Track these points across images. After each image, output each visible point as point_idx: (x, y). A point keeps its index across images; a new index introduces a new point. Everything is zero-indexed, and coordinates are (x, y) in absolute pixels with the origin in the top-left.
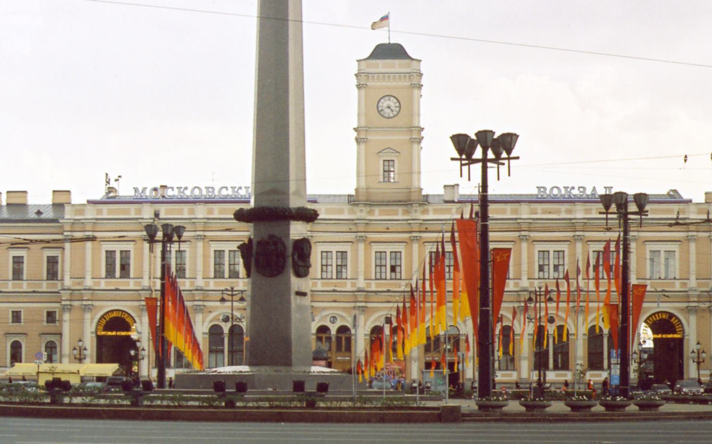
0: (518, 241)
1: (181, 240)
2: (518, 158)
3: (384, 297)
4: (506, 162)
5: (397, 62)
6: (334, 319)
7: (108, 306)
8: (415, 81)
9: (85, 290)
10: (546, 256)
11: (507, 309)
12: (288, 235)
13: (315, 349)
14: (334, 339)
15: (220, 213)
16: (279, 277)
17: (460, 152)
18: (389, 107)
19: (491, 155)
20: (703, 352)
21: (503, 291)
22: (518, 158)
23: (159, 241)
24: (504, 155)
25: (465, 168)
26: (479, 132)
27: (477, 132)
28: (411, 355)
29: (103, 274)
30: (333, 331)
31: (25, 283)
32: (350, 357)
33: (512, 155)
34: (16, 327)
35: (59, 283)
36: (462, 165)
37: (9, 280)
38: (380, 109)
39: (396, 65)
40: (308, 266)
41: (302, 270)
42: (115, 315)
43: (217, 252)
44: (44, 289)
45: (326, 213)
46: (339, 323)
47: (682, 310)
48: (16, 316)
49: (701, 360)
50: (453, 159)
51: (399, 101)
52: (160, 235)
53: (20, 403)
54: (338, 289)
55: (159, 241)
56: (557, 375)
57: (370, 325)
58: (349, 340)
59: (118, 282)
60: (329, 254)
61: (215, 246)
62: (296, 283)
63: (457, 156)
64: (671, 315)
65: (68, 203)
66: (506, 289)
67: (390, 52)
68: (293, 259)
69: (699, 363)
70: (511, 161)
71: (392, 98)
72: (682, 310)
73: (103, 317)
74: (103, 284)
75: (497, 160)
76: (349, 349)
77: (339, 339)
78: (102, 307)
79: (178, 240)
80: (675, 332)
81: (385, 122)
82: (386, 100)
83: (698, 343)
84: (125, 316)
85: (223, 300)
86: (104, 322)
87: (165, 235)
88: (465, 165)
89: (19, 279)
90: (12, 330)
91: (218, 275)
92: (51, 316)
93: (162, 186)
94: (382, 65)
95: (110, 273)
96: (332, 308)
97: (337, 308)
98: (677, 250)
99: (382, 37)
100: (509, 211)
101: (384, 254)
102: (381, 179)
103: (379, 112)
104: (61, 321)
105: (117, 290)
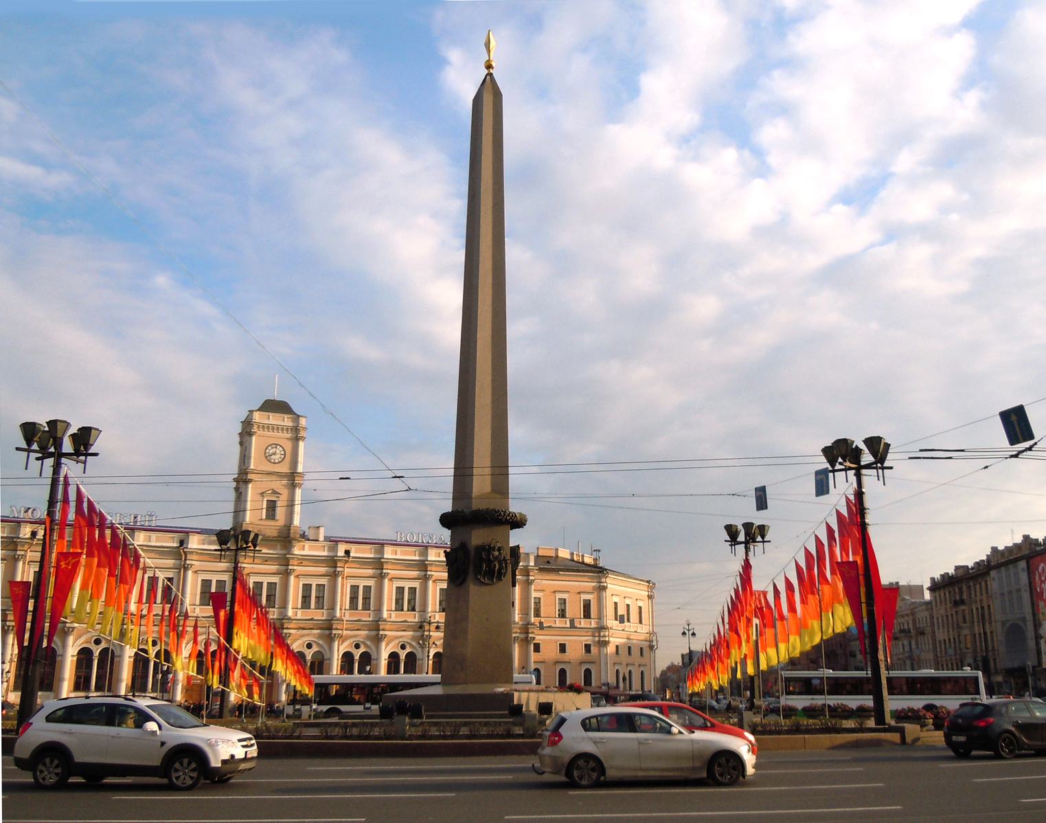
1: (765, 540)
5: (286, 416)
6: (403, 647)
10: (309, 588)
12: (471, 542)
13: (54, 639)
22: (769, 541)
23: (741, 543)
24: (759, 539)
27: (823, 447)
28: (844, 608)
33: (765, 540)
38: (267, 455)
39: (287, 421)
43: (413, 590)
45: (355, 552)
50: (726, 541)
51: (284, 450)
52: (741, 538)
53: (359, 737)
55: (741, 543)
60: (322, 587)
61: (303, 581)
63: (729, 539)
70: (885, 470)
71: (278, 447)
82: (273, 448)
87: (747, 534)
91: (322, 587)
94: (274, 419)
101: (223, 583)
103: (266, 457)
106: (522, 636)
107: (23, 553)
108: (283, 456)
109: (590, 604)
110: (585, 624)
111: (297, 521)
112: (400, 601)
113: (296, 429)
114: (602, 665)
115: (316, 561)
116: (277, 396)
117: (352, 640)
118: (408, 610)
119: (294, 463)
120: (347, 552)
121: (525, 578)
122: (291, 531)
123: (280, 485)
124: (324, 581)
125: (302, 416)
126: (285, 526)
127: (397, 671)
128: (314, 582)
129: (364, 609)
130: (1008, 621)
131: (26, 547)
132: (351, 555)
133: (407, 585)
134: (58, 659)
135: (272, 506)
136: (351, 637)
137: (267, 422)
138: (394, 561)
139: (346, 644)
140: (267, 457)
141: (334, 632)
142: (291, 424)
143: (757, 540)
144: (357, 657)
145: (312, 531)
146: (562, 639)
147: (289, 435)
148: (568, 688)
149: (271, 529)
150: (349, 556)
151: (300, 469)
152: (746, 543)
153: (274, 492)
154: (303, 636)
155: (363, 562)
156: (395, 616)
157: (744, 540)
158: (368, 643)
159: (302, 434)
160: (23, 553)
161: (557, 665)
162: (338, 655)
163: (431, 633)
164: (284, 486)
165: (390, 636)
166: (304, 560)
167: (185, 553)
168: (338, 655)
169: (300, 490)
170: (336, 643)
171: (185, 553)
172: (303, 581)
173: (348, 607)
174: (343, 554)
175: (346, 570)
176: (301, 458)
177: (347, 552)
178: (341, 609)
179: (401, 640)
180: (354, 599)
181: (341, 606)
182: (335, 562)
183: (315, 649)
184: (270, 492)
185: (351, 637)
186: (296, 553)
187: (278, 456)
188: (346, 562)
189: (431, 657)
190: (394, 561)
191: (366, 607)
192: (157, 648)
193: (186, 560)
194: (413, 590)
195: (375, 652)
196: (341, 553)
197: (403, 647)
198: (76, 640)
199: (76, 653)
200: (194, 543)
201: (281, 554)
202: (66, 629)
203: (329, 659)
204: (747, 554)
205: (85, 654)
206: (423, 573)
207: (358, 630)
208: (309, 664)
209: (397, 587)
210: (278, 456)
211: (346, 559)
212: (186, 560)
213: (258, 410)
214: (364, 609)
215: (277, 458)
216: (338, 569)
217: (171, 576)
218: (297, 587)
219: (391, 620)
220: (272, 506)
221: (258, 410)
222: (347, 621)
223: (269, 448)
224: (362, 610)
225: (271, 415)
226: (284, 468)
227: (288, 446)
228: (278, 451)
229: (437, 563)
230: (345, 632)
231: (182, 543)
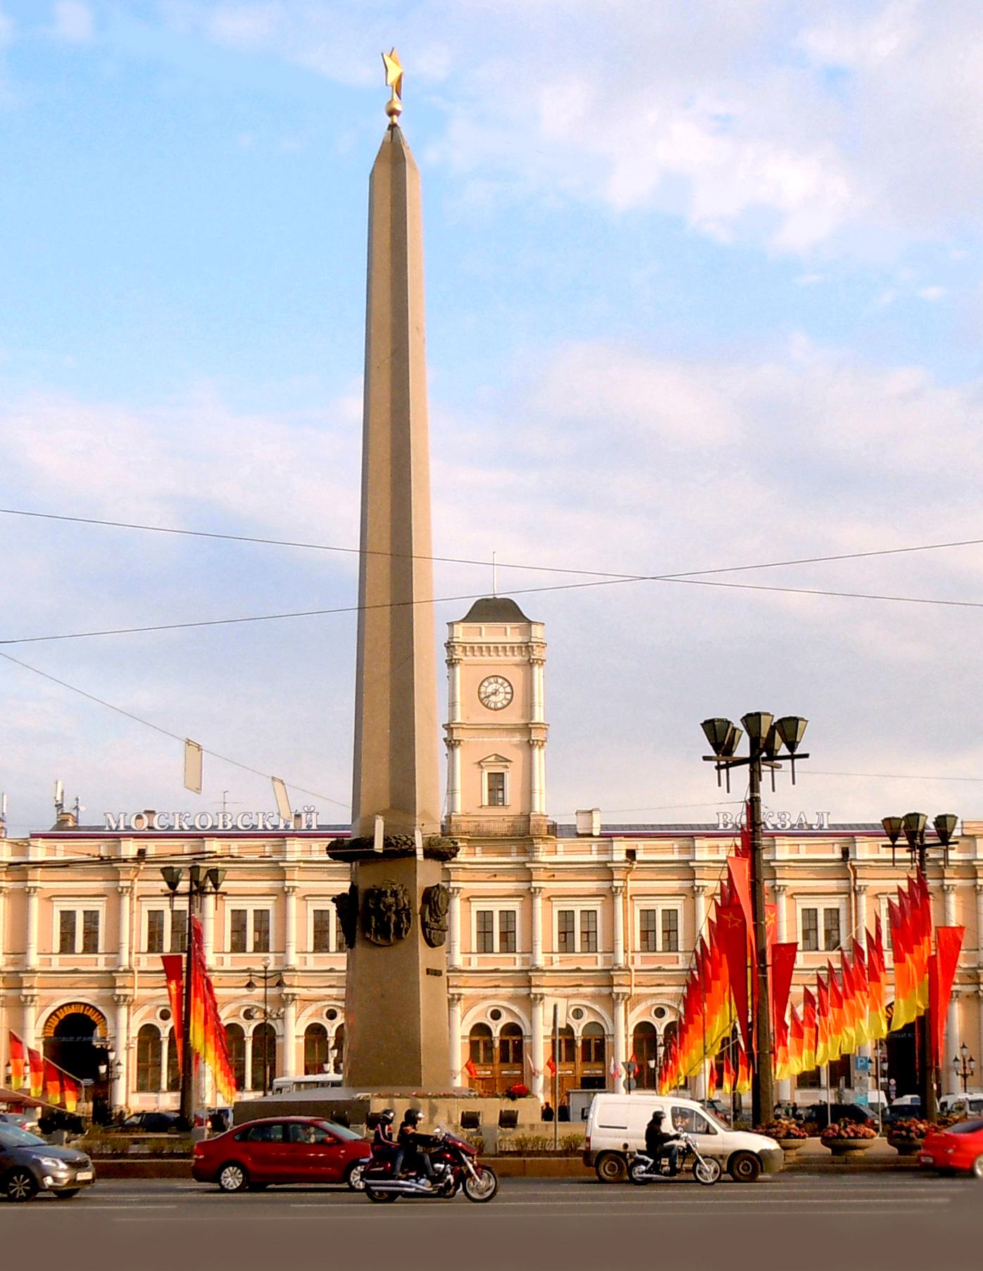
0: (528, 897)
1: (796, 753)
2: (806, 756)
4: (786, 764)
5: (509, 626)
6: (496, 1015)
7: (61, 997)
8: (529, 657)
9: (27, 972)
16: (402, 945)
17: (716, 746)
18: (494, 694)
20: (971, 1060)
21: (793, 969)
22: (806, 756)
24: (783, 750)
25: (723, 772)
26: (749, 715)
29: (57, 948)
30: (496, 1033)
32: (604, 1070)
33: (796, 753)
36: (719, 768)
39: (509, 633)
40: (444, 930)
41: (436, 934)
42: (73, 1010)
43: (813, 913)
46: (505, 1019)
49: (968, 1072)
50: (705, 758)
52: (743, 749)
56: (142, 1100)
57: (636, 1017)
58: (519, 1049)
59: (79, 959)
62: (426, 956)
63: (713, 754)
66: (796, 966)
68: (423, 919)
69: (965, 1076)
70: (796, 761)
73: (54, 1013)
74: (57, 962)
75: (772, 757)
76: (519, 1057)
77: (504, 1044)
78: (52, 999)
79: (788, 753)
83: (964, 1047)
84: (89, 1013)
85: (250, 985)
86: (55, 1022)
88: (723, 767)
93: (146, 812)
94: (490, 632)
95: (67, 945)
102: (486, 802)
103: (481, 700)
106: (970, 989)
107: (128, 884)
108: (509, 696)
110: (315, 963)
111: (540, 806)
112: (812, 934)
113: (527, 647)
115: (580, 870)
116: (500, 591)
117: (650, 1002)
118: (827, 949)
119: (529, 706)
120: (631, 854)
121: (969, 883)
122: (532, 823)
123: (508, 745)
124: (835, 903)
125: (536, 623)
126: (521, 815)
128: (577, 907)
129: (257, 949)
131: (132, 874)
132: (638, 857)
133: (821, 904)
134: (278, 1041)
135: (497, 781)
138: (712, 865)
139: (640, 1009)
140: (484, 701)
141: (616, 990)
142: (519, 639)
143: (779, 754)
144: (660, 1031)
145: (583, 818)
147: (518, 658)
148: (922, 1089)
149: (499, 820)
150: (634, 859)
151: (539, 717)
152: (753, 761)
153: (501, 759)
154: (485, 998)
155: (661, 868)
156: (558, 962)
157: (747, 755)
158: (516, 1009)
159: (537, 654)
160: (128, 884)
162: (627, 1029)
164: (516, 745)
165: (467, 998)
166: (554, 872)
167: (853, 867)
168: (627, 1029)
169: (543, 751)
170: (622, 1008)
171: (853, 867)
172: (231, 904)
173: (638, 948)
174: (623, 857)
175: (630, 884)
176: (539, 698)
177: (631, 854)
178: (625, 951)
179: (245, 1001)
180: (647, 935)
181: (626, 945)
182: (610, 870)
183: (587, 1018)
184: (492, 759)
186: (543, 859)
187: (502, 696)
188: (629, 870)
189: (631, 1031)
190: (712, 865)
191: (91, 947)
192: (254, 1024)
193: (855, 878)
194: (91, 917)
195: (527, 1024)
196: (620, 856)
199: (302, 1033)
200: (865, 851)
201: (598, 862)
202: (23, 999)
203: (531, 1037)
204: (754, 787)
206: (688, 884)
207: (659, 985)
208: (579, 1044)
209: (233, 911)
210: (502, 696)
211: (627, 865)
212: (855, 878)
213: (464, 620)
214: (257, 949)
215: (499, 700)
216: (616, 883)
217: (836, 906)
219: (307, 968)
220: (497, 781)
221: (464, 620)
222: (140, 972)
223: (486, 684)
224: (664, 951)
225: (483, 626)
226: (513, 717)
227: (517, 676)
228: (501, 690)
229: (792, 864)
230: (636, 991)
231: (845, 852)
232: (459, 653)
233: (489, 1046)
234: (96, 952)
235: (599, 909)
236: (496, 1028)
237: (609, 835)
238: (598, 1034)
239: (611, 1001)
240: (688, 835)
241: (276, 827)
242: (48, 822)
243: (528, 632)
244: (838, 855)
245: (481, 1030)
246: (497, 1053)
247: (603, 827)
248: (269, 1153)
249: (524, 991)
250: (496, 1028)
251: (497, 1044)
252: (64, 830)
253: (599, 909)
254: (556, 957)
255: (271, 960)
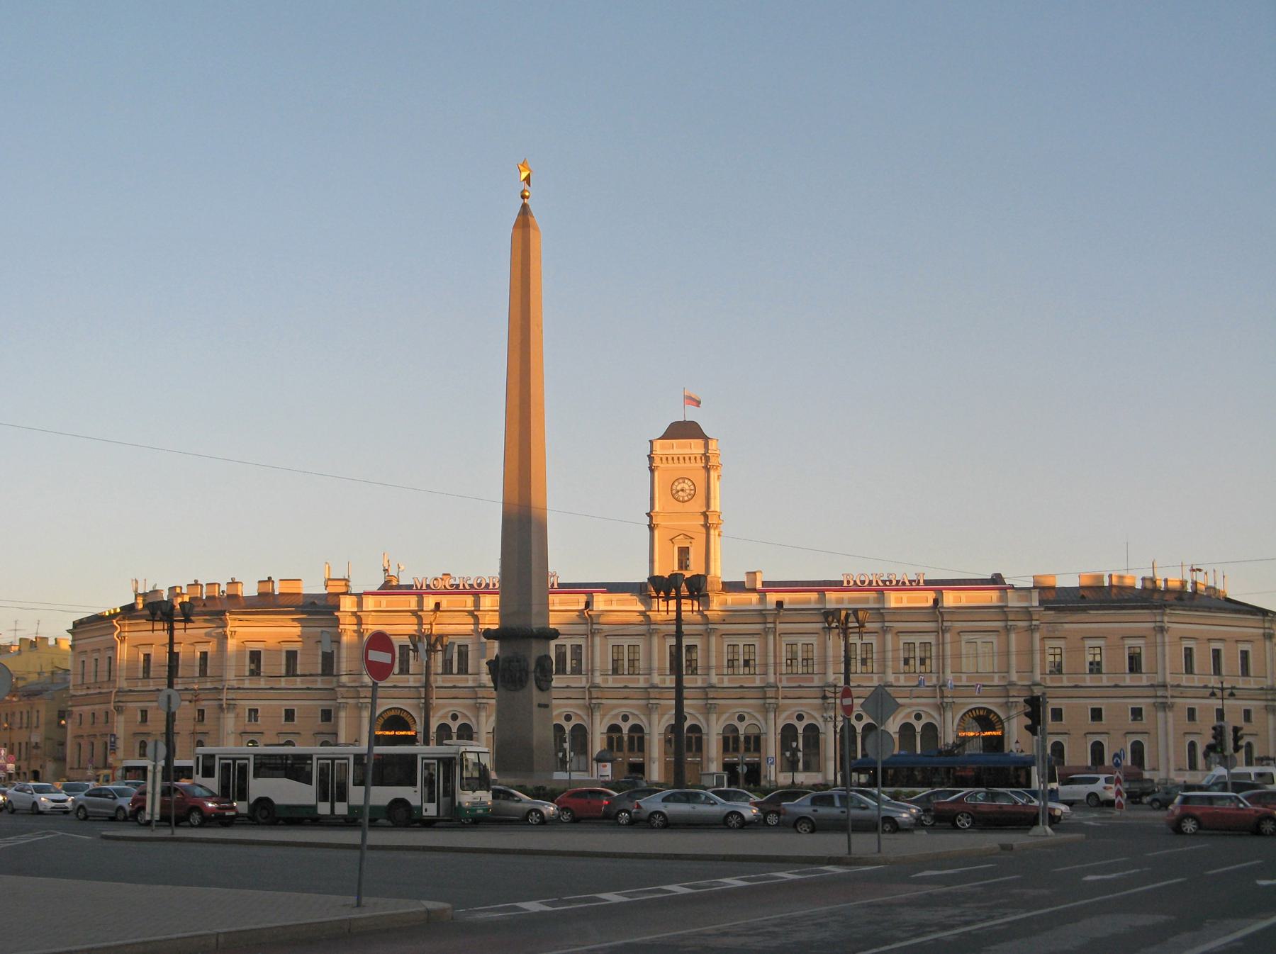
3: (567, 693)
11: (692, 706)
14: (626, 738)
15: (561, 604)
19: (662, 594)
29: (141, 675)
30: (625, 730)
31: (1104, 677)
34: (1096, 726)
35: (335, 679)
37: (317, 675)
39: (696, 446)
42: (393, 713)
44: (319, 686)
47: (1001, 705)
48: (290, 715)
54: (630, 685)
57: (607, 722)
58: (641, 740)
61: (728, 641)
64: (990, 711)
65: (345, 593)
67: (683, 430)
72: (1001, 705)
76: (641, 749)
77: (631, 739)
80: (409, 730)
81: (679, 507)
84: (404, 715)
89: (331, 674)
90: (249, 729)
92: (327, 715)
96: (566, 706)
97: (571, 706)
98: (995, 641)
99: (691, 414)
100: (905, 599)
104: (337, 717)
105: (454, 687)
109: (332, 658)
113: (706, 457)
114: (1161, 733)
115: (762, 614)
127: (736, 749)
129: (574, 671)
130: (339, 649)
135: (684, 552)
136: (910, 705)
137: (671, 452)
144: (918, 729)
146: (1096, 703)
161: (1129, 736)
163: (781, 701)
177: (438, 605)
185: (910, 705)
195: (763, 722)
197: (918, 717)
198: (718, 720)
205: (788, 733)
213: (662, 438)
218: (661, 651)
220: (684, 552)
221: (662, 438)
227: (699, 477)
231: (588, 604)
232: (657, 463)
233: (620, 739)
234: (466, 673)
235: (933, 642)
236: (625, 728)
237: (770, 586)
238: (757, 731)
239: (591, 709)
240: (476, 592)
241: (863, 582)
242: (376, 582)
243: (706, 446)
244: (930, 603)
245: (614, 729)
246: (626, 745)
247: (764, 583)
248: (115, 817)
249: (938, 700)
250: (625, 728)
251: (626, 738)
252: (389, 588)
253: (933, 642)
254: (610, 678)
255: (582, 681)
